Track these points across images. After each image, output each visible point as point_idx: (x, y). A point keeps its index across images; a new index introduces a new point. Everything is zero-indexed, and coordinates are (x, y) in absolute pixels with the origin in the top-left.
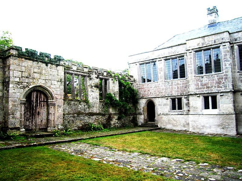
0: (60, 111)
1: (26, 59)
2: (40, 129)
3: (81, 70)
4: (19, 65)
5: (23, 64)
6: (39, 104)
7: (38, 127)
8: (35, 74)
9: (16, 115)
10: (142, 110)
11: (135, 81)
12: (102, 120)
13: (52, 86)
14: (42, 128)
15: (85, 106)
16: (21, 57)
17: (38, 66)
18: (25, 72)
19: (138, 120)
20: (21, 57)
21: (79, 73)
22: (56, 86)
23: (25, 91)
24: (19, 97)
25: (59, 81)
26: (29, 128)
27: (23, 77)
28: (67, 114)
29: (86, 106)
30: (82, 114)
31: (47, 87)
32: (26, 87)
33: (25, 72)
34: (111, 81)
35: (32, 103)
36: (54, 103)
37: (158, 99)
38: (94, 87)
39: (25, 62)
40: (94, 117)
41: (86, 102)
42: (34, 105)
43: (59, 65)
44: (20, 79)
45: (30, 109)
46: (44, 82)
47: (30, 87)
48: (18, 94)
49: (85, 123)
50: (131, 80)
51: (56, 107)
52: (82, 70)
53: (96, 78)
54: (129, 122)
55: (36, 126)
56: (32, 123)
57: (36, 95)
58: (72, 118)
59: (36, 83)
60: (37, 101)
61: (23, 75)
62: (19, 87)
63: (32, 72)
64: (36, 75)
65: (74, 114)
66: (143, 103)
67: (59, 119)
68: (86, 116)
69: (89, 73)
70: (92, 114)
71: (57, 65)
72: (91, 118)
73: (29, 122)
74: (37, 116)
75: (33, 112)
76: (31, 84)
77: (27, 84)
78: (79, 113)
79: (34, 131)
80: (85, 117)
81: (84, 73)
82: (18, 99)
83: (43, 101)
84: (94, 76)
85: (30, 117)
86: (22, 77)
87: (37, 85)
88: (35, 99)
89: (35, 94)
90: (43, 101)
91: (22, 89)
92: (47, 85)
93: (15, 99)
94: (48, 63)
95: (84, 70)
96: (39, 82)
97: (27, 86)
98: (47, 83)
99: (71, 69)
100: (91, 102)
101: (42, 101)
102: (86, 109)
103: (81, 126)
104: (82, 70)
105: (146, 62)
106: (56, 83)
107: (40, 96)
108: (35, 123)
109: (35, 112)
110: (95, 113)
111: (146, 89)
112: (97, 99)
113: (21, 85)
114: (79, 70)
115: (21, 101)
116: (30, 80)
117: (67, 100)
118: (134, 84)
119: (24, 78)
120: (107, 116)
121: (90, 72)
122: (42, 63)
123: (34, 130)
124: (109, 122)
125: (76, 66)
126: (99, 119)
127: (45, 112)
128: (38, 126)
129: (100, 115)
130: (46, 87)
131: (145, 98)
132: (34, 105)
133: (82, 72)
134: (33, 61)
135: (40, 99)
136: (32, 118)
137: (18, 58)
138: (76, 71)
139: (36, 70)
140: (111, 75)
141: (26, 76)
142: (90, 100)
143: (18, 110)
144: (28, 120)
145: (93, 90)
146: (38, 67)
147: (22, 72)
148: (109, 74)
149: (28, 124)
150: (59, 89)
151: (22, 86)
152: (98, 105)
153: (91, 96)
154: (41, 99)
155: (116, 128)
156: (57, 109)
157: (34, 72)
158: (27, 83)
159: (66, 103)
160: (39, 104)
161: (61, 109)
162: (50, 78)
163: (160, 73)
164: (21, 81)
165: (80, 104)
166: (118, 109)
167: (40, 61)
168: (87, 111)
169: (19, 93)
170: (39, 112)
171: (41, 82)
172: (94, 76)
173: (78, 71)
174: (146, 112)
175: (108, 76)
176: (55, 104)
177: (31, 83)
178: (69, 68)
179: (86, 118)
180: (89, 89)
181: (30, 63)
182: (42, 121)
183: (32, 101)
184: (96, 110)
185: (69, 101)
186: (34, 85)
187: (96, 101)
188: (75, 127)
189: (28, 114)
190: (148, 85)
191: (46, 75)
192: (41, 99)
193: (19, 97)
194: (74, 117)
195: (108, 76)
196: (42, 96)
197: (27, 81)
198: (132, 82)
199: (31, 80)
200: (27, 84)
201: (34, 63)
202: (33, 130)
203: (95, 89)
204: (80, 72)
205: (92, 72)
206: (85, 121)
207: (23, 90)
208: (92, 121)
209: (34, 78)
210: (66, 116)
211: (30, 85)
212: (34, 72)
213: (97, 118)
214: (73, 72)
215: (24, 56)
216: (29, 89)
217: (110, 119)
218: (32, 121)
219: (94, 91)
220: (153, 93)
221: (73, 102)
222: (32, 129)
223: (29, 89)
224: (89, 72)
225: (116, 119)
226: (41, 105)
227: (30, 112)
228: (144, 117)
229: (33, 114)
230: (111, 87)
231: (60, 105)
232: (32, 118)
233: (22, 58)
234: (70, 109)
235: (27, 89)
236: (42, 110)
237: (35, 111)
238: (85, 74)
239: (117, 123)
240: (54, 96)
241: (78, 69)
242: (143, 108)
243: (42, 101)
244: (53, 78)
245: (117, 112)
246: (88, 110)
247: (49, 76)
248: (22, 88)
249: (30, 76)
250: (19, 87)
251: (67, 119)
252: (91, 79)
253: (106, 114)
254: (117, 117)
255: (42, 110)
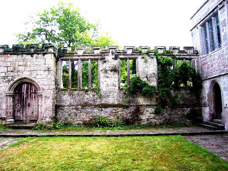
0: (48, 103)
1: (11, 54)
2: (31, 121)
3: (89, 53)
4: (5, 61)
5: (9, 60)
6: (29, 96)
7: (29, 119)
8: (20, 67)
9: (2, 106)
10: (207, 98)
11: (198, 53)
12: (123, 113)
13: (38, 77)
14: (34, 119)
15: (94, 96)
16: (6, 54)
17: (23, 58)
18: (10, 67)
19: (203, 115)
20: (6, 54)
21: (87, 57)
22: (42, 76)
23: (10, 85)
24: (4, 90)
25: (46, 71)
26: (20, 119)
27: (9, 71)
28: (68, 106)
29: (96, 96)
30: (90, 105)
31: (32, 79)
32: (11, 80)
33: (10, 67)
34: (142, 60)
35: (22, 95)
36: (41, 94)
37: (223, 79)
38: (109, 72)
39: (11, 58)
40: (109, 110)
41: (97, 90)
42: (25, 97)
43: (46, 53)
44: (5, 74)
45: (21, 101)
46: (29, 73)
47: (15, 80)
48: (4, 87)
49: (94, 116)
50: (186, 53)
51: (43, 98)
52: (90, 53)
53: (113, 60)
54: (181, 117)
55: (26, 117)
56: (22, 114)
57: (26, 87)
58: (75, 111)
59: (21, 75)
60: (27, 93)
61: (8, 70)
62: (5, 81)
63: (17, 65)
64: (21, 68)
65: (78, 105)
66: (207, 85)
67: (48, 111)
68: (94, 108)
69: (101, 55)
70: (106, 106)
71: (44, 54)
72: (103, 110)
73: (20, 113)
74: (28, 107)
75: (23, 103)
76: (16, 77)
77: (12, 78)
78: (85, 105)
79: (24, 122)
80: (94, 110)
81: (94, 56)
82: (3, 92)
83: (33, 93)
84: (110, 58)
85: (21, 108)
86: (7, 71)
87: (22, 77)
88: (25, 91)
89: (25, 86)
90: (33, 93)
91: (7, 83)
92: (32, 76)
93: (1, 92)
94: (34, 54)
95: (93, 53)
96: (24, 75)
97: (12, 79)
98: (32, 74)
99: (74, 55)
100: (104, 91)
101: (33, 93)
102: (97, 99)
103: (88, 120)
104: (90, 53)
105: (207, 18)
106: (42, 72)
107: (31, 88)
108: (25, 114)
109: (25, 104)
110: (110, 105)
111: (209, 63)
112: (116, 86)
113: (6, 79)
114: (87, 53)
115: (6, 94)
116: (15, 73)
117: (69, 90)
118: (195, 59)
119: (9, 72)
120: (132, 109)
121: (104, 54)
122: (27, 55)
123: (25, 121)
124: (137, 116)
125: (82, 50)
126: (118, 112)
127: (37, 103)
128: (29, 118)
129: (120, 107)
130: (31, 78)
131: (209, 79)
132: (25, 97)
133: (92, 56)
134: (18, 54)
135: (30, 91)
136: (23, 110)
137: (4, 55)
138: (83, 56)
139: (20, 63)
140: (140, 52)
141: (11, 70)
142: (103, 87)
143: (3, 102)
144: (19, 112)
145: (108, 75)
146: (23, 59)
147: (8, 67)
148: (137, 52)
149: (19, 115)
150: (46, 79)
151: (8, 80)
152: (116, 94)
153: (105, 83)
154: (32, 91)
155: (150, 125)
156: (45, 100)
157: (19, 66)
158: (12, 76)
159: (67, 93)
160: (29, 96)
161: (49, 101)
162: (35, 68)
163: (223, 30)
164: (7, 75)
165: (87, 94)
166: (157, 99)
167: (25, 54)
168: (98, 102)
169: (4, 87)
170: (29, 104)
171: (26, 74)
172: (110, 58)
173: (84, 56)
174: (212, 102)
175: (134, 54)
176: (42, 95)
177: (16, 76)
178: (72, 54)
179: (96, 110)
180: (102, 75)
181: (15, 57)
182: (33, 112)
183: (23, 93)
184: (111, 100)
185: (71, 91)
186: (19, 78)
187: (112, 89)
188: (80, 121)
189: (18, 106)
190: (211, 56)
191: (31, 66)
192: (32, 91)
193: (4, 90)
194: (77, 109)
195: (134, 54)
196: (33, 88)
197: (12, 75)
198: (190, 55)
199: (16, 74)
200: (12, 78)
201: (19, 56)
202: (24, 121)
203: (111, 74)
204: (88, 56)
205: (107, 53)
206: (95, 114)
207: (8, 83)
208: (105, 114)
209: (18, 71)
210: (66, 107)
211: (14, 78)
212: (19, 66)
213: (114, 111)
214: (79, 58)
215: (9, 52)
216: (13, 82)
217: (138, 111)
218: (23, 112)
219: (110, 76)
220: (217, 69)
221: (76, 92)
222: (22, 121)
223: (13, 82)
224: (102, 53)
225: (152, 113)
226: (32, 97)
227: (21, 104)
228: (210, 110)
229: (23, 106)
230: (142, 68)
231: (48, 96)
232: (23, 110)
233: (7, 54)
234: (72, 100)
235: (12, 82)
236: (32, 102)
237: (26, 103)
238: (97, 57)
239: (155, 118)
240: (41, 86)
241: (84, 53)
242: (208, 95)
243: (33, 93)
244: (39, 68)
245: (155, 102)
246: (99, 100)
247: (34, 67)
248: (7, 82)
249: (15, 69)
250: (5, 81)
251: (67, 111)
252: (105, 62)
253: (131, 106)
254: (153, 110)
255: (32, 102)
